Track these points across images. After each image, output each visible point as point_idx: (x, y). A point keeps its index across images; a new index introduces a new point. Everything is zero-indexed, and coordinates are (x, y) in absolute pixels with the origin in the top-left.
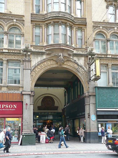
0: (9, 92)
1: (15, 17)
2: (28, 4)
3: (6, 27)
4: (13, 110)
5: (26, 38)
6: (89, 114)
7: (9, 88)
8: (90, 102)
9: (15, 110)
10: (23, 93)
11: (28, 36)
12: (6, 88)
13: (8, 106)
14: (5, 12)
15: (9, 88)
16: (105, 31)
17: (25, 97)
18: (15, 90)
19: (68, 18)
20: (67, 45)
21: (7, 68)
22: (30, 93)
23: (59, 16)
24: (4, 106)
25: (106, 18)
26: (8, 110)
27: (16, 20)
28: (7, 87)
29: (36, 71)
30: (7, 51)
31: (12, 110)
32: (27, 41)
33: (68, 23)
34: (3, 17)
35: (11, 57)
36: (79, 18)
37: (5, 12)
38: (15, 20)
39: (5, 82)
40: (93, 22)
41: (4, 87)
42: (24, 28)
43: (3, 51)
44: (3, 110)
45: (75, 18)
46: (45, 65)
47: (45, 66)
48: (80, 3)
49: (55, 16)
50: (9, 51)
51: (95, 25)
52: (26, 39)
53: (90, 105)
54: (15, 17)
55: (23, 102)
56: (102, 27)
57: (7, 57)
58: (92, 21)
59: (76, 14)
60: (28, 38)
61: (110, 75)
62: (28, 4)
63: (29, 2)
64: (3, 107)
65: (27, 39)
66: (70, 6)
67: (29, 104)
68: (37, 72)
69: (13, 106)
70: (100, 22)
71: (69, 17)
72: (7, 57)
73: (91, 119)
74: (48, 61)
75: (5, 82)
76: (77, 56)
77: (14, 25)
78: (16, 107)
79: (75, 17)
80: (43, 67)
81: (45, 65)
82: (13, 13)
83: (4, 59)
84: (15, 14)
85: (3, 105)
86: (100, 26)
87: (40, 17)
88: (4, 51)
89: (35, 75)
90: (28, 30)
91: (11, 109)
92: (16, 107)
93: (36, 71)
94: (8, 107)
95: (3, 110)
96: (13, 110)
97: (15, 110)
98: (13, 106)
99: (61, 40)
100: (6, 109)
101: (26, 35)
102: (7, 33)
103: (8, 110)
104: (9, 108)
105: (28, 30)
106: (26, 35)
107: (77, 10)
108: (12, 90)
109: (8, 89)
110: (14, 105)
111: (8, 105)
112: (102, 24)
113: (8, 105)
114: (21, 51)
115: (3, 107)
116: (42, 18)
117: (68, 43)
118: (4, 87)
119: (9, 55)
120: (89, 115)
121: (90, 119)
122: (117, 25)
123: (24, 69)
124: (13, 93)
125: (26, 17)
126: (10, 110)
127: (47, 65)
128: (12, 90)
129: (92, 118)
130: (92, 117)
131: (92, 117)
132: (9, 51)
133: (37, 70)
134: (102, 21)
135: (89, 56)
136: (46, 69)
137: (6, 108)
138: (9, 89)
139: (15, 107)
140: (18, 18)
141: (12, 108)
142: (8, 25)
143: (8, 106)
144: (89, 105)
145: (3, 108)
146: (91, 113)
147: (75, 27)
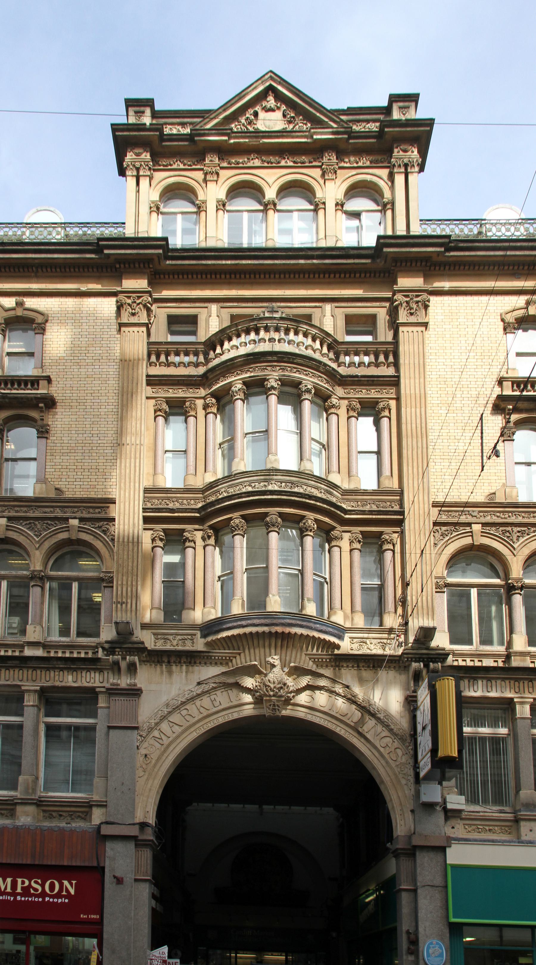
0: (47, 824)
1: (75, 507)
2: (133, 450)
3: (37, 553)
4: (60, 901)
5: (119, 593)
6: (412, 937)
7: (45, 808)
8: (420, 880)
9: (67, 901)
10: (106, 830)
11: (129, 583)
12: (31, 809)
13: (43, 886)
14: (37, 491)
15: (45, 808)
16: (495, 545)
17: (112, 849)
18: (72, 816)
19: (310, 497)
20: (308, 618)
21: (42, 728)
22: (134, 831)
23: (270, 488)
24: (23, 883)
25: (504, 485)
26: (40, 900)
27: (81, 520)
28: (39, 803)
29: (163, 737)
30: (39, 652)
31: (56, 900)
32: (124, 606)
33: (311, 516)
34: (26, 512)
35: (57, 678)
36: (365, 492)
37: (37, 491)
38: (75, 522)
39: (31, 785)
40: (435, 505)
41: (25, 802)
42: (113, 552)
43: (22, 654)
44: (19, 898)
45: (347, 492)
46: (202, 710)
47: (205, 713)
48: (377, 424)
49: (250, 489)
50: (49, 652)
51: (444, 518)
52: (120, 600)
53: (419, 891)
54: (75, 507)
55: (103, 868)
56: (484, 525)
57: (39, 677)
58: (431, 500)
59: (354, 472)
60: (129, 594)
61: (522, 754)
62: (133, 450)
63: (138, 442)
64: (19, 890)
65: (124, 600)
66: (324, 441)
67: (129, 878)
68: (166, 741)
69: (61, 885)
70: (467, 505)
71: (316, 493)
72: (39, 677)
73: (421, 958)
74: (218, 693)
75: (31, 785)
76: (395, 667)
77: (69, 542)
78: (72, 892)
79: (345, 486)
80: (196, 719)
81: (202, 710)
82: (69, 495)
83: (27, 685)
84: (78, 495)
85: (19, 880)
86: (470, 519)
87: (185, 502)
88: (28, 652)
89: (158, 753)
90: (130, 560)
91: (51, 896)
92: (72, 892)
93: (163, 737)
94: (33, 884)
95: (19, 898)
96: (60, 901)
97: (67, 901)
98: (61, 885)
99: (277, 598)
100: (31, 895)
101: (120, 583)
102: (41, 579)
103: (40, 900)
104: (43, 894)
105: (130, 560)
106: (120, 583)
107: (360, 455)
108: (61, 815)
109: (44, 811)
110: (66, 883)
111: (39, 881)
112: (480, 512)
113: (39, 881)
114: (100, 650)
115: (19, 890)
116: (192, 502)
117: (311, 609)
118: (25, 802)
119: (48, 669)
120: (414, 942)
121: (417, 957)
122: (534, 512)
123: (110, 728)
124: (62, 830)
125: (122, 506)
126: (47, 899)
127: (215, 710)
128: (61, 815)
129: (428, 955)
130: (428, 948)
131: (428, 948)
132: (49, 652)
133: (169, 733)
134: (480, 497)
135: (414, 665)
136: (211, 725)
137: (32, 891)
138: (47, 815)
139: (67, 890)
140: (89, 513)
141: (59, 895)
142: (47, 545)
143: (43, 886)
144: (415, 891)
145: (19, 894)
146: (421, 929)
147: (346, 536)
